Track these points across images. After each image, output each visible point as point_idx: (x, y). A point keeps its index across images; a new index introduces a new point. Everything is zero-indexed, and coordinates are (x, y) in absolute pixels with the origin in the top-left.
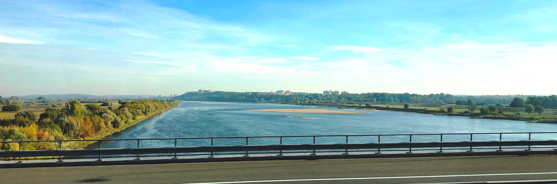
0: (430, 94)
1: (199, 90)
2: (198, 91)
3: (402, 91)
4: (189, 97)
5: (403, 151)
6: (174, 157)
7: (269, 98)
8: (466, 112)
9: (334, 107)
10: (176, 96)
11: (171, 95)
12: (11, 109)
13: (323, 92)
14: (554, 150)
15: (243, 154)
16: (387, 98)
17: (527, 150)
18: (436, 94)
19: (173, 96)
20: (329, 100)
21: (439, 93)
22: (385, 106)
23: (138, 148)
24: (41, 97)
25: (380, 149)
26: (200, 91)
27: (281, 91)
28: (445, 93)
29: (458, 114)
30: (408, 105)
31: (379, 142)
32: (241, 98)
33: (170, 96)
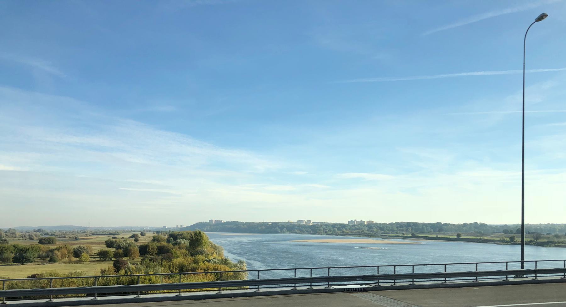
0: (464, 223)
3: (434, 221)
5: (439, 281)
7: (291, 228)
8: (531, 241)
9: (374, 237)
11: (177, 226)
12: (48, 242)
13: (348, 221)
14: (561, 278)
17: (563, 278)
18: (469, 223)
19: (179, 227)
20: (361, 230)
21: (472, 222)
22: (435, 236)
23: (3, 290)
24: (40, 229)
25: (379, 281)
26: (211, 221)
27: (302, 221)
28: (479, 222)
30: (461, 234)
31: (445, 271)
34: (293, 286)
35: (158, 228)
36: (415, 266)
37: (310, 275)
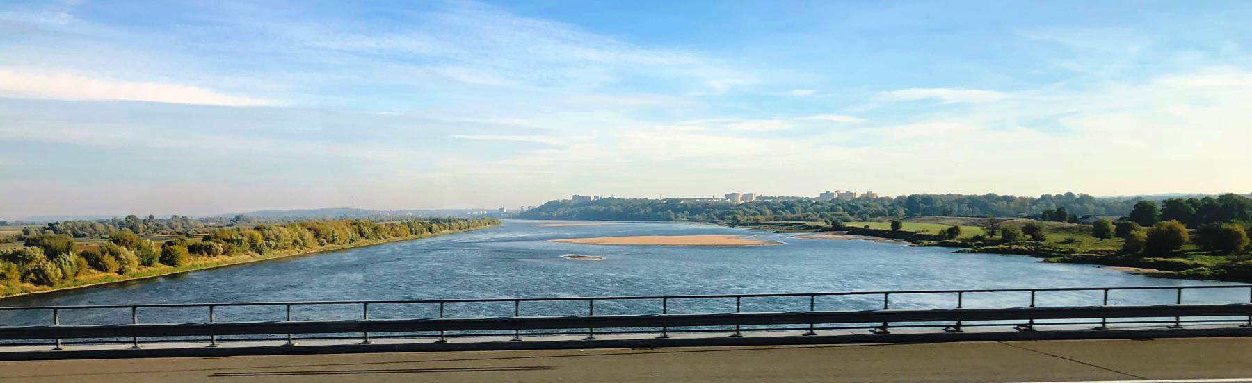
1: (821, 194)
2: (571, 199)
4: (553, 210)
5: (864, 329)
6: (589, 336)
10: (531, 208)
15: (658, 332)
16: (938, 206)
19: (526, 209)
21: (1063, 194)
22: (861, 225)
28: (637, 198)
29: (960, 242)
32: (642, 212)
33: (520, 209)
34: (661, 332)
35: (1126, 199)
36: (1109, 292)
37: (440, 314)
